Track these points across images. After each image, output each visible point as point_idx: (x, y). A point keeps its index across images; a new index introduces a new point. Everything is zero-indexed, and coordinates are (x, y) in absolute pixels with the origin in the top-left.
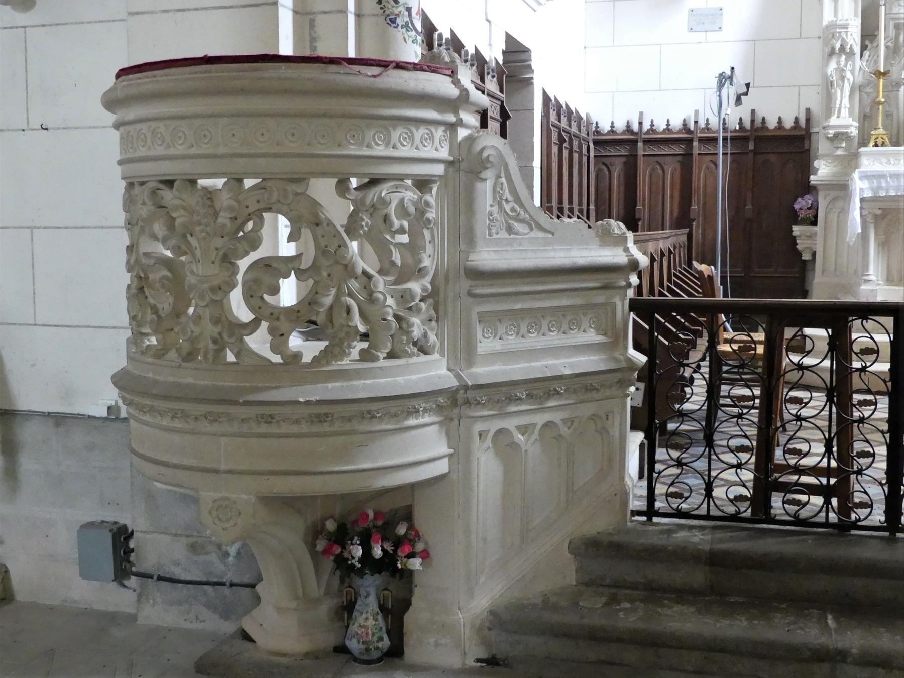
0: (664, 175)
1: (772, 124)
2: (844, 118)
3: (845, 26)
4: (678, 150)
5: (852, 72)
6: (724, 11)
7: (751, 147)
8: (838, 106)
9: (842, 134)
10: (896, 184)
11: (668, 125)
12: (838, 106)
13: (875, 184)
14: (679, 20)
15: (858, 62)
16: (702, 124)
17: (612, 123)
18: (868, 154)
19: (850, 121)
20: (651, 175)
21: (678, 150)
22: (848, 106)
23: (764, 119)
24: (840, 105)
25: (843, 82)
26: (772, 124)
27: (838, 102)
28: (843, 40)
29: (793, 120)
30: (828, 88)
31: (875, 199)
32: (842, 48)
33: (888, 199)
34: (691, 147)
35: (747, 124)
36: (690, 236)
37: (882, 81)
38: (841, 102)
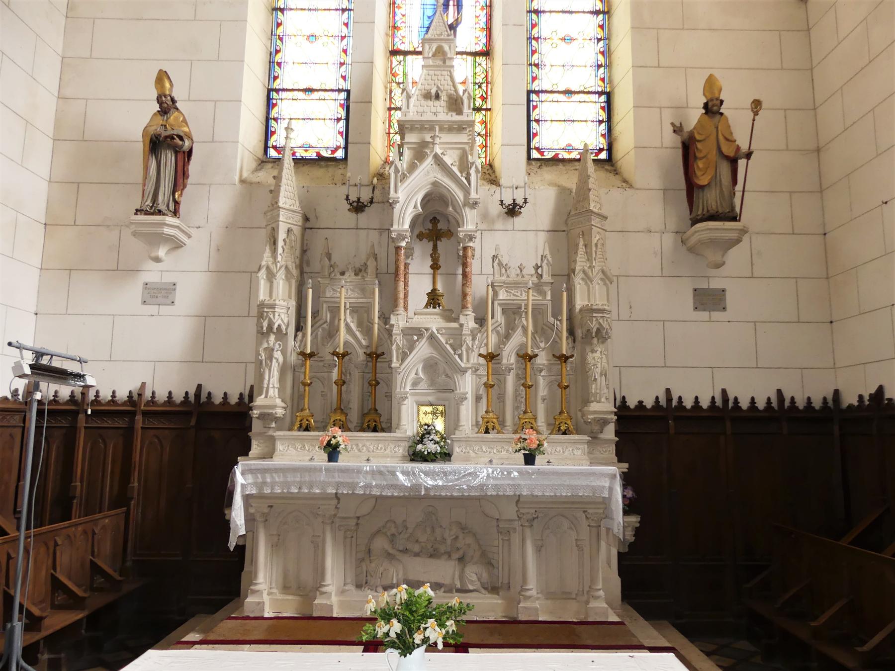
0: (106, 447)
1: (218, 399)
2: (272, 398)
3: (272, 307)
4: (121, 423)
5: (284, 352)
6: (178, 287)
7: (193, 422)
8: (265, 386)
9: (269, 414)
10: (282, 480)
11: (114, 396)
12: (265, 386)
13: (260, 480)
14: (133, 291)
15: (291, 342)
16: (148, 394)
17: (114, 392)
18: (283, 439)
19: (279, 402)
20: (92, 449)
21: (121, 423)
22: (277, 385)
23: (209, 394)
24: (268, 385)
25: (271, 361)
26: (218, 399)
27: (266, 382)
28: (270, 319)
29: (765, 401)
31: (261, 497)
32: (270, 327)
33: (273, 497)
34: (132, 421)
35: (192, 398)
36: (127, 514)
37: (308, 362)
38: (269, 381)
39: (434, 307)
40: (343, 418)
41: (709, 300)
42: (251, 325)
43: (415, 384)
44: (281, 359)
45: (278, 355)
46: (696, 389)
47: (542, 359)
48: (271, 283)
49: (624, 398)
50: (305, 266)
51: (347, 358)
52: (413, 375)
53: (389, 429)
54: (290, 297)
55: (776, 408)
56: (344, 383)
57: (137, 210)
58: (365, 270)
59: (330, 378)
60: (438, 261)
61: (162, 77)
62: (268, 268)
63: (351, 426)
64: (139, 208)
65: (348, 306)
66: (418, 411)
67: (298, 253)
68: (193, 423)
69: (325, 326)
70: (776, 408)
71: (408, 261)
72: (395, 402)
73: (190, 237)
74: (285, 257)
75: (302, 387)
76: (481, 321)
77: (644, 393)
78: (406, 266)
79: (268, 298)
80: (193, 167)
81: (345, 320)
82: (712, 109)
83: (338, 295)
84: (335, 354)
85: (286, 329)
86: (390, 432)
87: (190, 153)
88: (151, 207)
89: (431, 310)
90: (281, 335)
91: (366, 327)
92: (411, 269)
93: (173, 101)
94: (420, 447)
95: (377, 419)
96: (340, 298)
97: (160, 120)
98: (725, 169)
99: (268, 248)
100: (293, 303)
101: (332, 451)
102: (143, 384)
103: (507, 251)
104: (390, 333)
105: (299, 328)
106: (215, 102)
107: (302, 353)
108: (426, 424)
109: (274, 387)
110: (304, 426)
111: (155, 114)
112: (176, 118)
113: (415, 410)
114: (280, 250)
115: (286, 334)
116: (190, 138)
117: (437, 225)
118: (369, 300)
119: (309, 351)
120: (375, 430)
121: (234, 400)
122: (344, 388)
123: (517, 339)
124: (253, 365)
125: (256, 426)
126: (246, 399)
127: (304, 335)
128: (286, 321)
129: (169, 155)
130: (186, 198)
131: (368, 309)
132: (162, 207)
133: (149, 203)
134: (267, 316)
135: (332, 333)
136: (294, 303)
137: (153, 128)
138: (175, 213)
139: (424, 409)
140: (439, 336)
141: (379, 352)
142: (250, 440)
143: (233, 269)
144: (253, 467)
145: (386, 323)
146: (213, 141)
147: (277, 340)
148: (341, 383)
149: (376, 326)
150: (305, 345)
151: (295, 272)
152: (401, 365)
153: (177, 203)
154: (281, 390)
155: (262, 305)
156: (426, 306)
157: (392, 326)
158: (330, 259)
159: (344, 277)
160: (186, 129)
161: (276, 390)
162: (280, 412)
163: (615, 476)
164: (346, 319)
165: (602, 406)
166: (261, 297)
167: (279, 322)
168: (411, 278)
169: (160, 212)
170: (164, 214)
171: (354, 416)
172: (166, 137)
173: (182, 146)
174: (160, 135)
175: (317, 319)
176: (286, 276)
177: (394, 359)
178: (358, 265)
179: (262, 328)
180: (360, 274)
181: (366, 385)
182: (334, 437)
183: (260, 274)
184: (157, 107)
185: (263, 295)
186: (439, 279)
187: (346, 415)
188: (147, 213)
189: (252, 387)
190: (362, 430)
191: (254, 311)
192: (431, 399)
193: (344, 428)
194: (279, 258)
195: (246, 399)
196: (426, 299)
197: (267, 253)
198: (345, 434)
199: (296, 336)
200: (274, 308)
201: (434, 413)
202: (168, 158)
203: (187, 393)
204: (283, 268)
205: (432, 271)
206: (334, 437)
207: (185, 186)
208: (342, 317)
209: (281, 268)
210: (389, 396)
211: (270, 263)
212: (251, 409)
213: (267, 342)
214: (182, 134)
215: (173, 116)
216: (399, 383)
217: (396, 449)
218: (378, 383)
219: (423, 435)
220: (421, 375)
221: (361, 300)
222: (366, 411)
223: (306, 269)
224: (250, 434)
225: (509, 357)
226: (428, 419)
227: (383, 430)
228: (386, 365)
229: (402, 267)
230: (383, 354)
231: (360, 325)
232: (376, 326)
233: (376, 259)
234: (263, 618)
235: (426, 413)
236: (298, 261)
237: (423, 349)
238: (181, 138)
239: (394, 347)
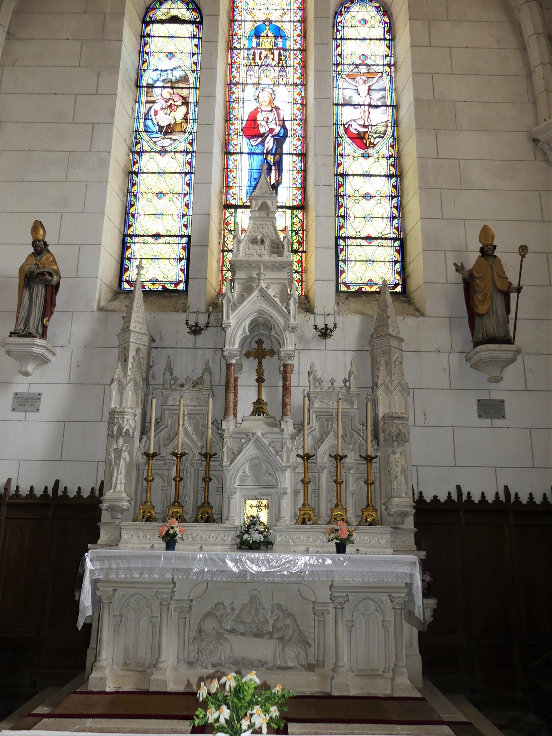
8: (114, 482)
27: (114, 478)
30: (109, 467)
41: (491, 409)
44: (128, 459)
46: (481, 486)
47: (351, 458)
49: (421, 493)
52: (241, 473)
57: (11, 333)
61: (37, 226)
64: (13, 331)
73: (54, 354)
74: (132, 370)
76: (300, 428)
77: (438, 489)
80: (60, 298)
82: (487, 252)
87: (57, 286)
88: (23, 331)
93: (46, 245)
94: (246, 536)
97: (33, 260)
98: (499, 301)
101: (170, 541)
102: (9, 480)
103: (323, 364)
106: (80, 245)
111: (30, 255)
112: (48, 259)
116: (58, 273)
117: (262, 346)
123: (330, 441)
129: (40, 288)
130: (54, 323)
132: (33, 331)
133: (21, 327)
137: (28, 266)
138: (43, 336)
143: (87, 382)
144: (101, 555)
146: (77, 277)
153: (45, 327)
160: (55, 267)
163: (415, 563)
165: (403, 501)
169: (30, 335)
170: (34, 337)
172: (39, 274)
173: (51, 281)
174: (33, 272)
184: (32, 250)
188: (19, 336)
202: (40, 291)
207: (52, 313)
214: (51, 271)
215: (44, 257)
217: (226, 538)
225: (323, 456)
234: (105, 693)
237: (249, 451)
238: (51, 275)
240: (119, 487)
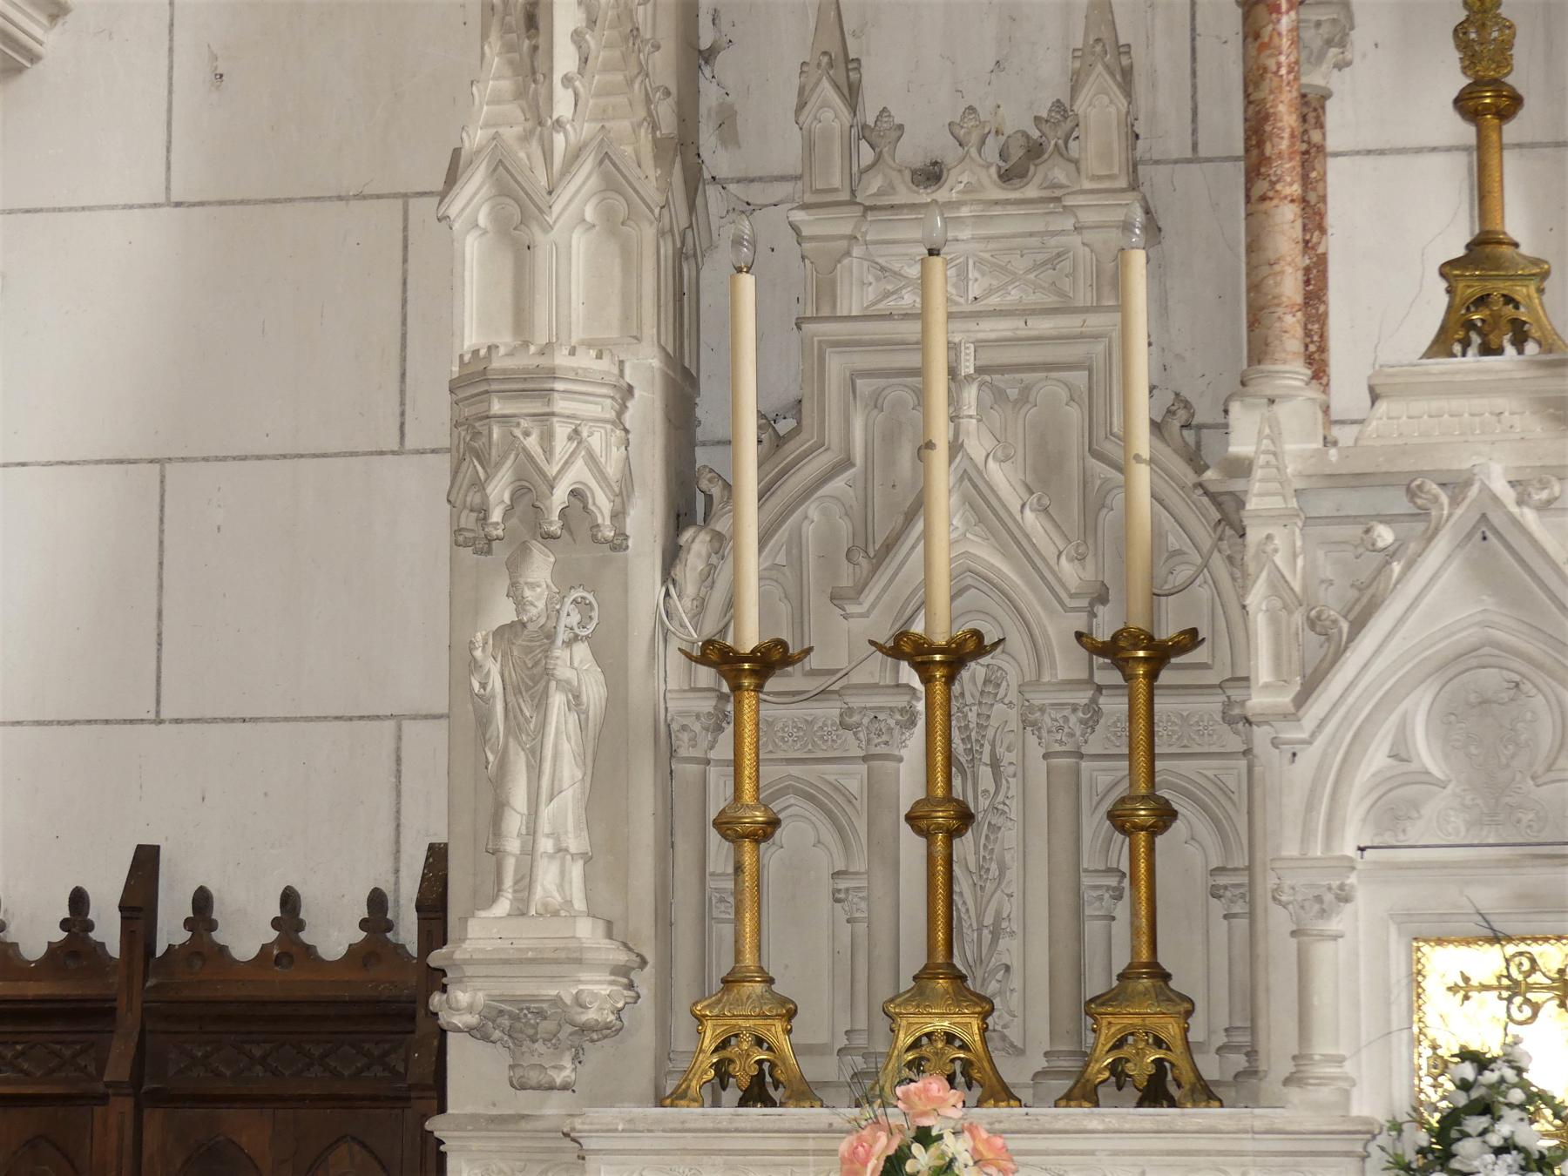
2: (550, 919)
3: (536, 384)
8: (513, 845)
24: (532, 831)
25: (541, 703)
27: (514, 823)
39: (1487, 350)
40: (968, 1027)
42: (416, 498)
43: (1393, 810)
44: (594, 691)
45: (576, 665)
48: (522, 253)
50: (708, 139)
51: (975, 671)
52: (1376, 759)
53: (1246, 1084)
54: (629, 316)
55: (114, 949)
56: (965, 817)
58: (1061, 152)
59: (878, 794)
60: (1503, 54)
62: (499, 165)
63: (1013, 1072)
65: (967, 367)
66: (1415, 978)
67: (663, 65)
68: (118, 1068)
69: (838, 484)
70: (114, 949)
71: (1315, 78)
72: (1278, 921)
75: (719, 851)
78: (1312, 107)
79: (505, 340)
81: (955, 448)
83: (909, 299)
84: (906, 648)
85: (618, 516)
86: (1253, 1101)
89: (1471, 363)
90: (583, 536)
91: (1075, 481)
92: (1339, 128)
95: (1171, 1030)
96: (921, 316)
99: (495, 59)
100: (645, 367)
104: (1228, 515)
105: (689, 503)
107: (718, 655)
108: (1466, 1055)
109: (560, 850)
110: (743, 1072)
113: (1398, 971)
114: (565, 59)
115: (619, 543)
118: (1095, 322)
119: (749, 638)
120: (1155, 1093)
121: (334, 934)
122: (964, 846)
124: (440, 730)
125: (472, 1075)
126: (407, 931)
127: (723, 544)
128: (612, 470)
131: (1100, 386)
134: (511, 443)
135: (881, 539)
136: (656, 362)
139: (1444, 963)
140: (1529, 517)
141: (1167, 631)
142: (442, 1158)
145: (1196, 460)
147: (565, 578)
148: (946, 820)
149: (1142, 477)
150: (732, 604)
151: (649, 179)
152: (1302, 699)
154: (604, 858)
155: (474, 381)
156: (1441, 345)
157: (1241, 468)
158: (852, 94)
159: (942, 194)
161: (576, 871)
162: (597, 992)
164: (969, 453)
166: (471, 338)
167: (578, 473)
168: (1339, 177)
171: (1029, 1017)
175: (792, 449)
176: (608, 215)
177: (1263, 671)
178: (1017, 119)
179: (483, 512)
180: (1038, 174)
181: (1095, 824)
182: (925, 1137)
183: (456, 205)
185: (476, 326)
186: (1514, 172)
187: (985, 1007)
189: (437, 857)
190: (1084, 1093)
191: (433, 416)
192: (1486, 896)
193: (981, 1081)
194: (563, 104)
195: (407, 931)
196: (1435, 303)
197: (495, 79)
198: (990, 1112)
199: (672, 555)
200: (546, 394)
201: (1513, 989)
203: (78, 900)
204: (588, 164)
205: (1467, 132)
206: (925, 1137)
208: (941, 433)
209: (574, 157)
210: (1237, 888)
211: (510, 134)
212: (436, 979)
213: (515, 593)
216: (1293, 803)
218: (1165, 816)
219: (1452, 1119)
220: (1427, 755)
221: (1045, 325)
222: (1096, 985)
223: (717, 160)
224: (436, 1125)
226: (1481, 1025)
227: (1205, 1093)
228: (1211, 705)
229: (1286, 117)
230: (1191, 639)
231: (1044, 475)
232: (1142, 477)
233: (1126, 78)
235: (1464, 988)
236: (666, 112)
237: (1433, 602)
239: (1257, 597)
240: (547, 880)
